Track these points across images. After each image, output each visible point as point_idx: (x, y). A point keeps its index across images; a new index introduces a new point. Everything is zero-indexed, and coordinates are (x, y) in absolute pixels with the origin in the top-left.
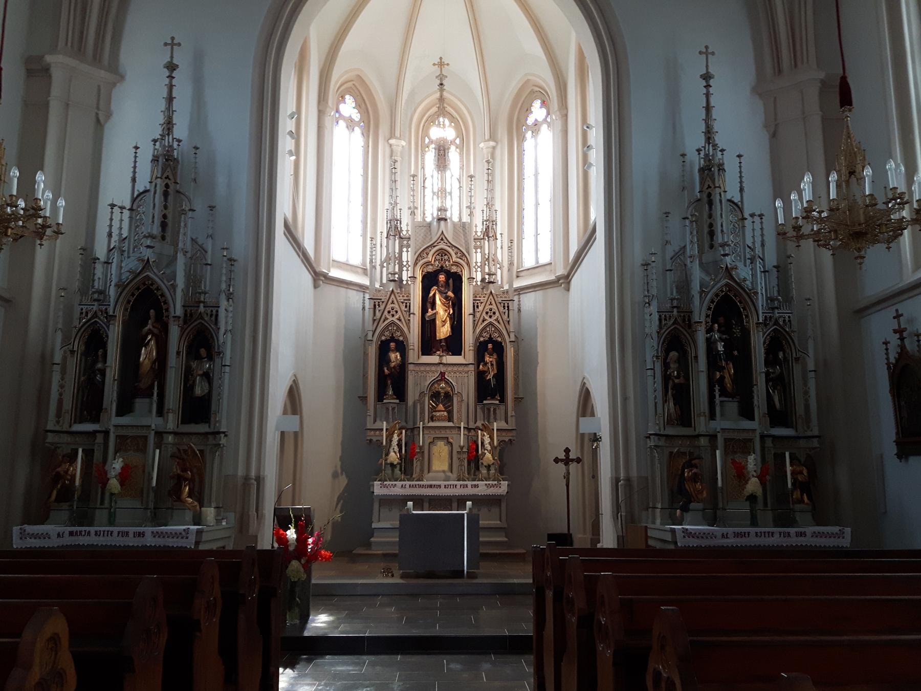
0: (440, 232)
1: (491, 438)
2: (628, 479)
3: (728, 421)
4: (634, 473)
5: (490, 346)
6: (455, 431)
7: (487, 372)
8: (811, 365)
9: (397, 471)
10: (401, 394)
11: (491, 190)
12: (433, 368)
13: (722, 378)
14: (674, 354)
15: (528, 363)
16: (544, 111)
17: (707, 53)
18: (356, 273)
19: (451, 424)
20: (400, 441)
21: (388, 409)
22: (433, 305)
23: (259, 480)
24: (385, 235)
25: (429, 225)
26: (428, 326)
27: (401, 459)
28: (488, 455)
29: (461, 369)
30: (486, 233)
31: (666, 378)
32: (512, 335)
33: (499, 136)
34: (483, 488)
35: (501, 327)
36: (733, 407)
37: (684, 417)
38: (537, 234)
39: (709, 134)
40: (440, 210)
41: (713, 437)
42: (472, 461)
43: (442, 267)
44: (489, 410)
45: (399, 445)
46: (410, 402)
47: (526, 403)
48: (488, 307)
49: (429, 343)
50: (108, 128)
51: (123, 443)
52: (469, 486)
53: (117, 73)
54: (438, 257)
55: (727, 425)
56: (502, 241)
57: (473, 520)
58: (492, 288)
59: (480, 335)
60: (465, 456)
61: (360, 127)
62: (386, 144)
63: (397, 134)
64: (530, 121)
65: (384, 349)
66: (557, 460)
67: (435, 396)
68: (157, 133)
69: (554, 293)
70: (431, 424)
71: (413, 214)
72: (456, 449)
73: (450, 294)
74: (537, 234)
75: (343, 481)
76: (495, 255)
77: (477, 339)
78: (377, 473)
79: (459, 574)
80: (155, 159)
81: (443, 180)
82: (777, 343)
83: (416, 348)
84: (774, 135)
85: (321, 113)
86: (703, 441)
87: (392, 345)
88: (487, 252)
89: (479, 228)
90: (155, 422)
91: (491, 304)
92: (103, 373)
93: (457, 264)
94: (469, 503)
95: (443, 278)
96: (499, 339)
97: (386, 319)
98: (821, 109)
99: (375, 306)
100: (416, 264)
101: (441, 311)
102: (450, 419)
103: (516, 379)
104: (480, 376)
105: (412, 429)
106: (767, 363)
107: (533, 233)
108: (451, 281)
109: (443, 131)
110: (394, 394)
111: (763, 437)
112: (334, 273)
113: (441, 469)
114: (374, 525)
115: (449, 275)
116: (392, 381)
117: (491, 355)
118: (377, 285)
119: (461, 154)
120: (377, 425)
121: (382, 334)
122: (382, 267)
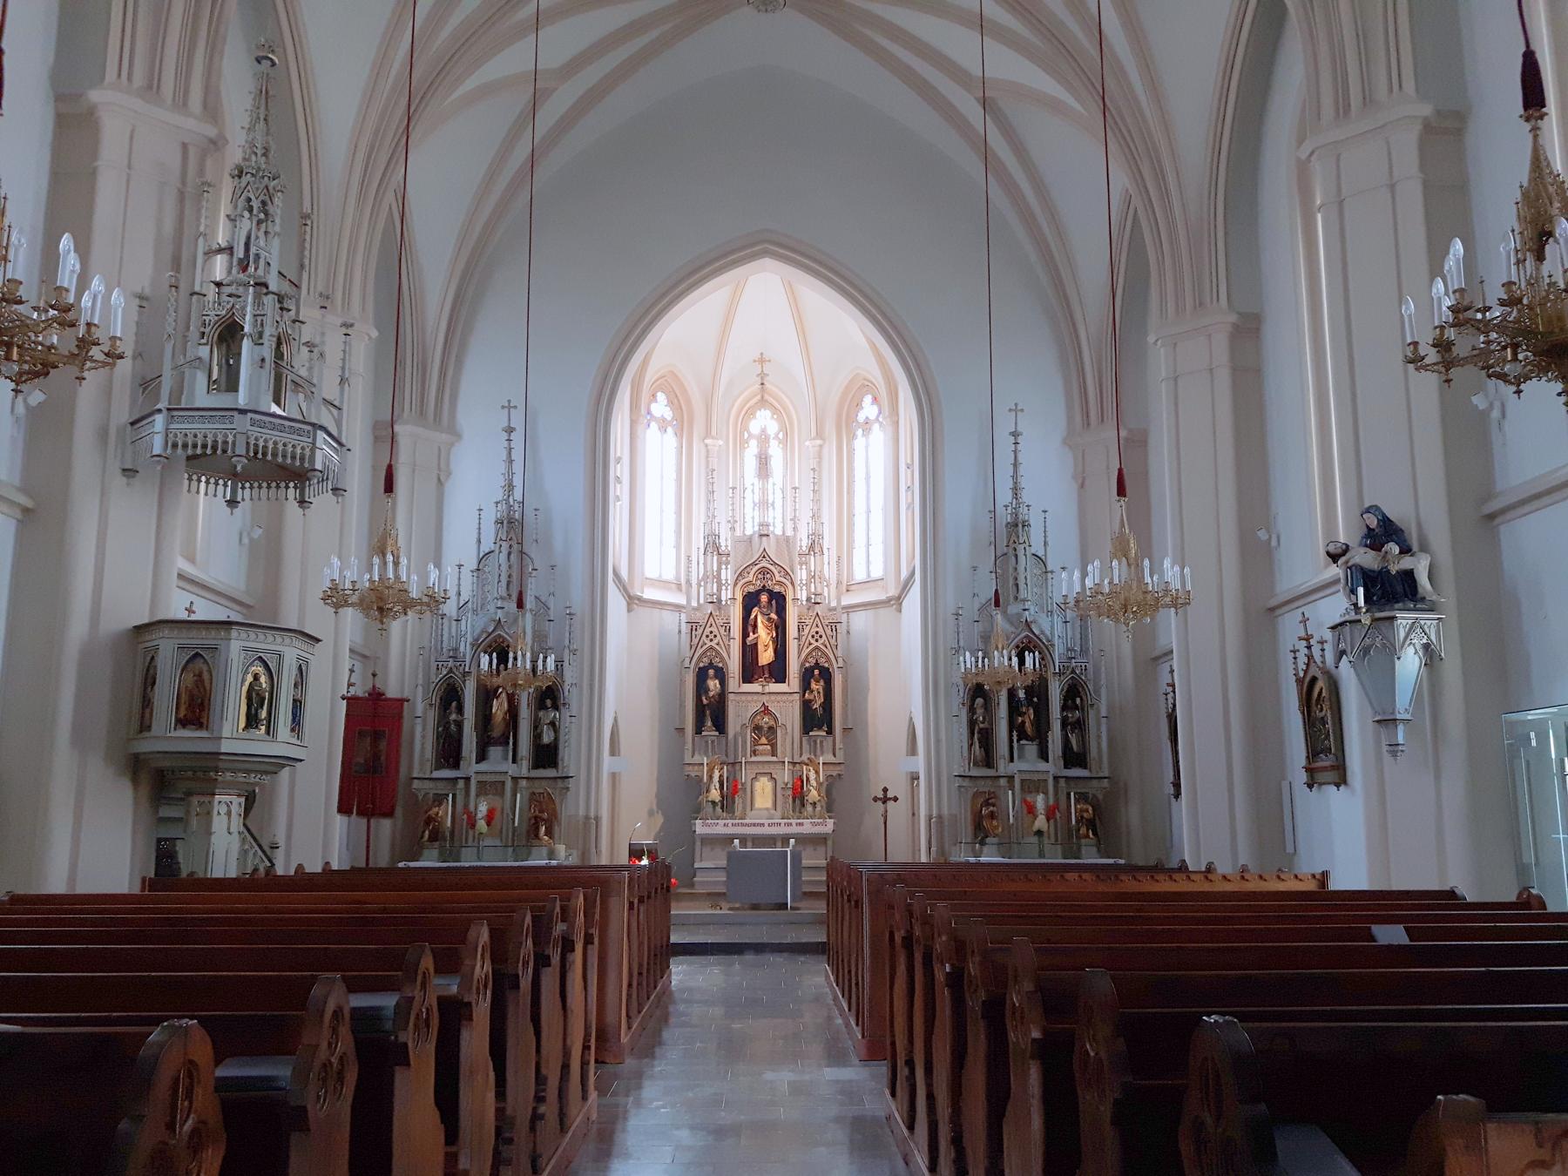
1: (817, 772)
2: (940, 817)
3: (1027, 763)
4: (945, 812)
6: (779, 766)
8: (1104, 713)
9: (718, 809)
10: (720, 725)
11: (817, 501)
13: (1023, 722)
14: (979, 701)
15: (858, 690)
17: (1016, 411)
18: (669, 589)
22: (755, 626)
23: (597, 819)
25: (750, 538)
26: (749, 652)
28: (814, 792)
29: (785, 697)
30: (811, 547)
31: (972, 723)
34: (808, 827)
36: (1031, 749)
37: (988, 760)
38: (868, 545)
39: (1016, 490)
40: (761, 525)
41: (1011, 778)
49: (750, 671)
50: (448, 486)
51: (484, 788)
53: (454, 432)
55: (1024, 766)
56: (830, 555)
57: (797, 858)
59: (806, 660)
60: (790, 792)
63: (714, 433)
64: (861, 417)
65: (702, 676)
66: (876, 799)
67: (757, 729)
68: (500, 495)
69: (886, 613)
71: (733, 529)
72: (780, 785)
73: (773, 616)
74: (868, 545)
75: (659, 820)
78: (697, 811)
79: (784, 906)
80: (499, 522)
81: (764, 491)
82: (1074, 692)
84: (1082, 486)
85: (633, 423)
86: (1003, 782)
87: (711, 672)
89: (805, 543)
90: (512, 769)
92: (459, 725)
93: (780, 583)
94: (792, 841)
95: (764, 599)
98: (1423, 167)
101: (764, 635)
102: (774, 754)
104: (806, 705)
105: (734, 764)
106: (1064, 708)
109: (764, 421)
111: (1056, 778)
112: (650, 594)
114: (696, 865)
116: (712, 713)
118: (694, 604)
119: (785, 449)
120: (697, 759)
121: (700, 659)
122: (699, 585)
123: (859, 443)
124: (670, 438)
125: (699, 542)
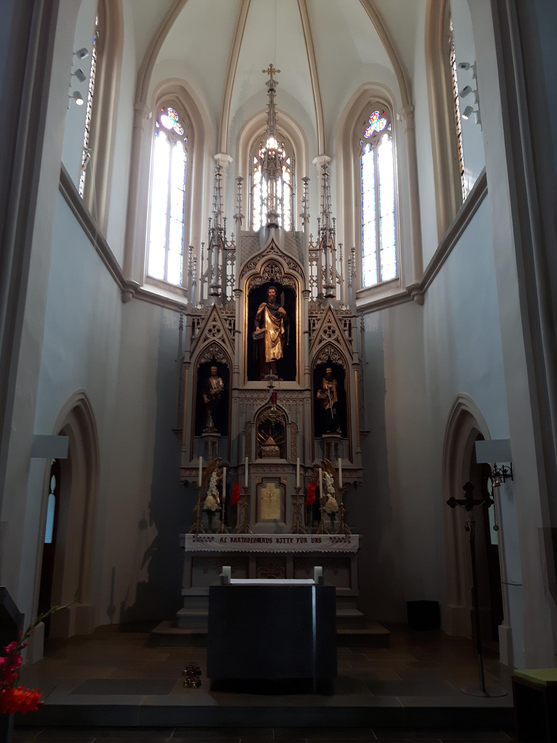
0: (270, 240)
1: (335, 478)
5: (329, 371)
6: (289, 470)
7: (326, 400)
9: (216, 519)
10: (223, 426)
11: (326, 197)
12: (262, 395)
15: (373, 389)
16: (384, 121)
18: (176, 293)
19: (283, 461)
20: (220, 482)
21: (206, 443)
22: (262, 323)
24: (207, 246)
25: (258, 234)
26: (256, 346)
27: (221, 505)
28: (332, 500)
29: (294, 396)
32: (355, 356)
33: (334, 149)
34: (326, 543)
35: (342, 347)
42: (311, 510)
43: (272, 280)
44: (329, 445)
45: (219, 487)
46: (234, 435)
47: (372, 435)
48: (326, 325)
49: (257, 366)
52: (309, 541)
54: (268, 269)
58: (330, 303)
59: (317, 357)
60: (302, 501)
61: (182, 141)
62: (211, 160)
63: (224, 149)
64: (369, 132)
65: (203, 373)
70: (259, 461)
73: (281, 310)
75: (152, 532)
76: (334, 266)
77: (313, 362)
83: (241, 371)
85: (137, 113)
87: (214, 369)
88: (323, 264)
89: (314, 238)
91: (329, 321)
93: (289, 276)
95: (273, 292)
96: (340, 362)
97: (206, 339)
99: (193, 323)
100: (241, 276)
102: (282, 454)
103: (361, 407)
105: (236, 468)
107: (374, 248)
108: (282, 295)
110: (215, 426)
112: (146, 288)
113: (272, 518)
114: (184, 592)
115: (280, 288)
116: (212, 410)
117: (330, 380)
121: (201, 355)
123: (367, 158)
124: (179, 151)
125: (204, 238)
